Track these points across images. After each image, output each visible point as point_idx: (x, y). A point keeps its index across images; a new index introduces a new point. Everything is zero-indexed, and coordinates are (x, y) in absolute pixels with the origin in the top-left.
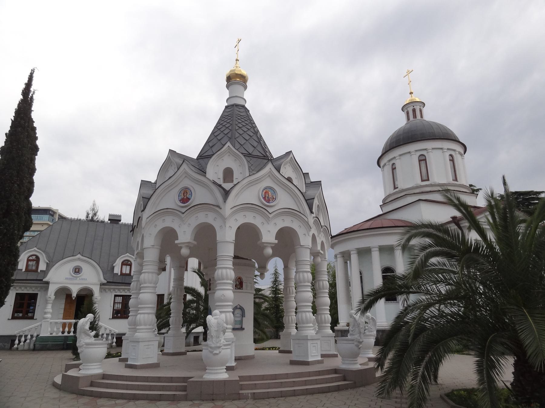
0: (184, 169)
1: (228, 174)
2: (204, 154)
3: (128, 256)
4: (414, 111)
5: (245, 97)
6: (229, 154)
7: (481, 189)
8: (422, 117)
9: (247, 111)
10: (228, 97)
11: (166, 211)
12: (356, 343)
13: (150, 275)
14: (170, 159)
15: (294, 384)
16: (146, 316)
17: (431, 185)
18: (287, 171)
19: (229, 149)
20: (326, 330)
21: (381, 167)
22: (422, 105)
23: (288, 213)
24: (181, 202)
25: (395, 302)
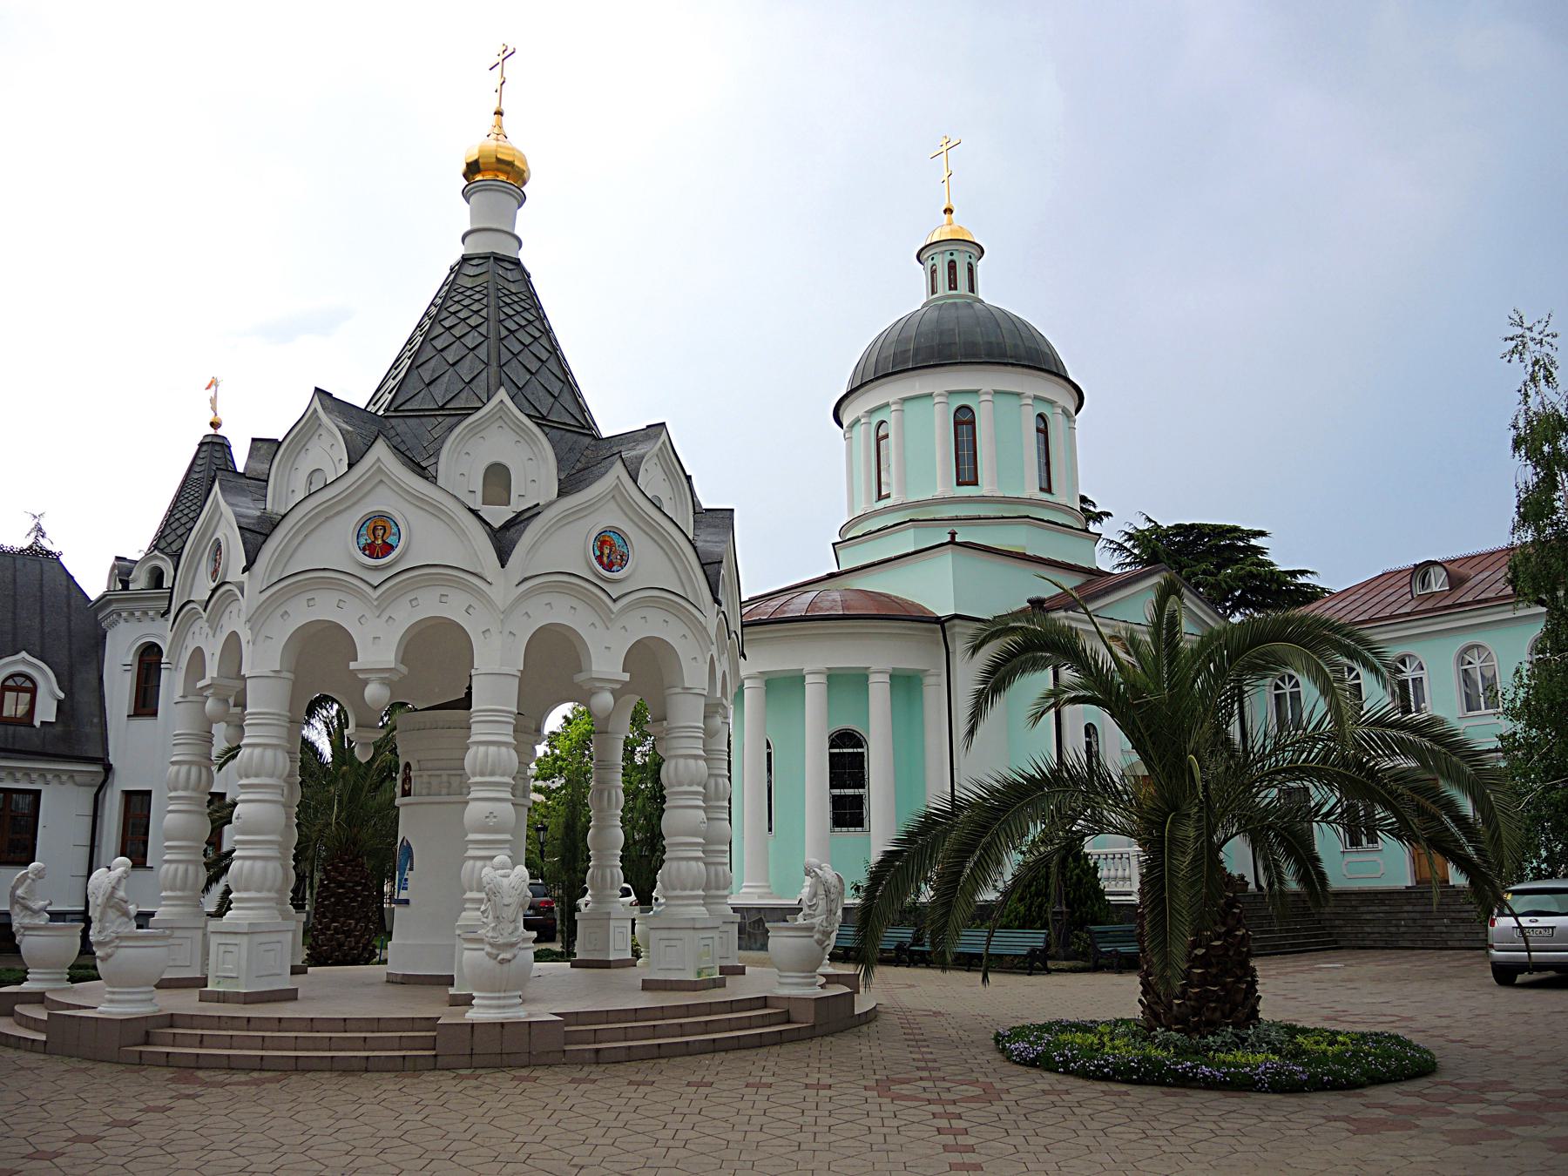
0: (379, 459)
1: (497, 478)
2: (408, 403)
3: (24, 661)
4: (952, 266)
5: (517, 232)
6: (500, 423)
7: (1108, 514)
8: (972, 289)
9: (525, 277)
10: (468, 228)
11: (322, 579)
12: (817, 936)
13: (269, 753)
14: (318, 418)
15: (682, 1030)
16: (259, 864)
17: (983, 500)
18: (652, 478)
19: (501, 408)
20: (719, 907)
21: (845, 427)
22: (976, 253)
23: (656, 601)
24: (367, 552)
25: (860, 829)
